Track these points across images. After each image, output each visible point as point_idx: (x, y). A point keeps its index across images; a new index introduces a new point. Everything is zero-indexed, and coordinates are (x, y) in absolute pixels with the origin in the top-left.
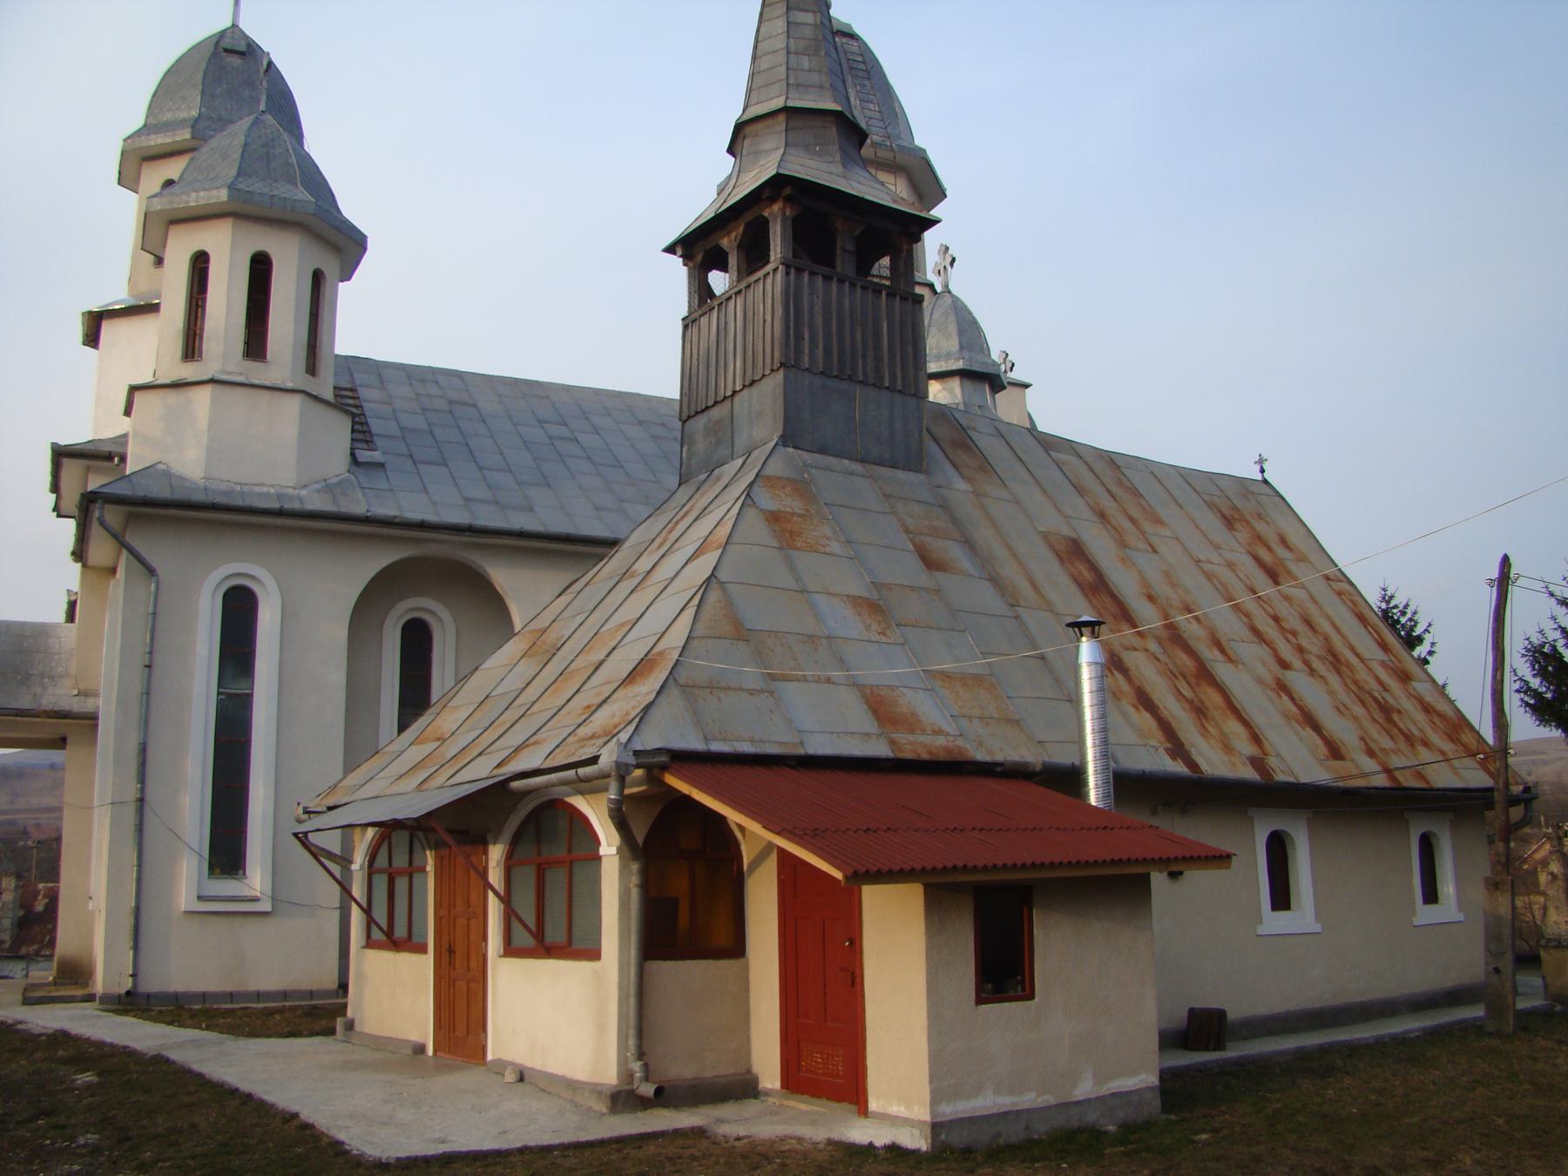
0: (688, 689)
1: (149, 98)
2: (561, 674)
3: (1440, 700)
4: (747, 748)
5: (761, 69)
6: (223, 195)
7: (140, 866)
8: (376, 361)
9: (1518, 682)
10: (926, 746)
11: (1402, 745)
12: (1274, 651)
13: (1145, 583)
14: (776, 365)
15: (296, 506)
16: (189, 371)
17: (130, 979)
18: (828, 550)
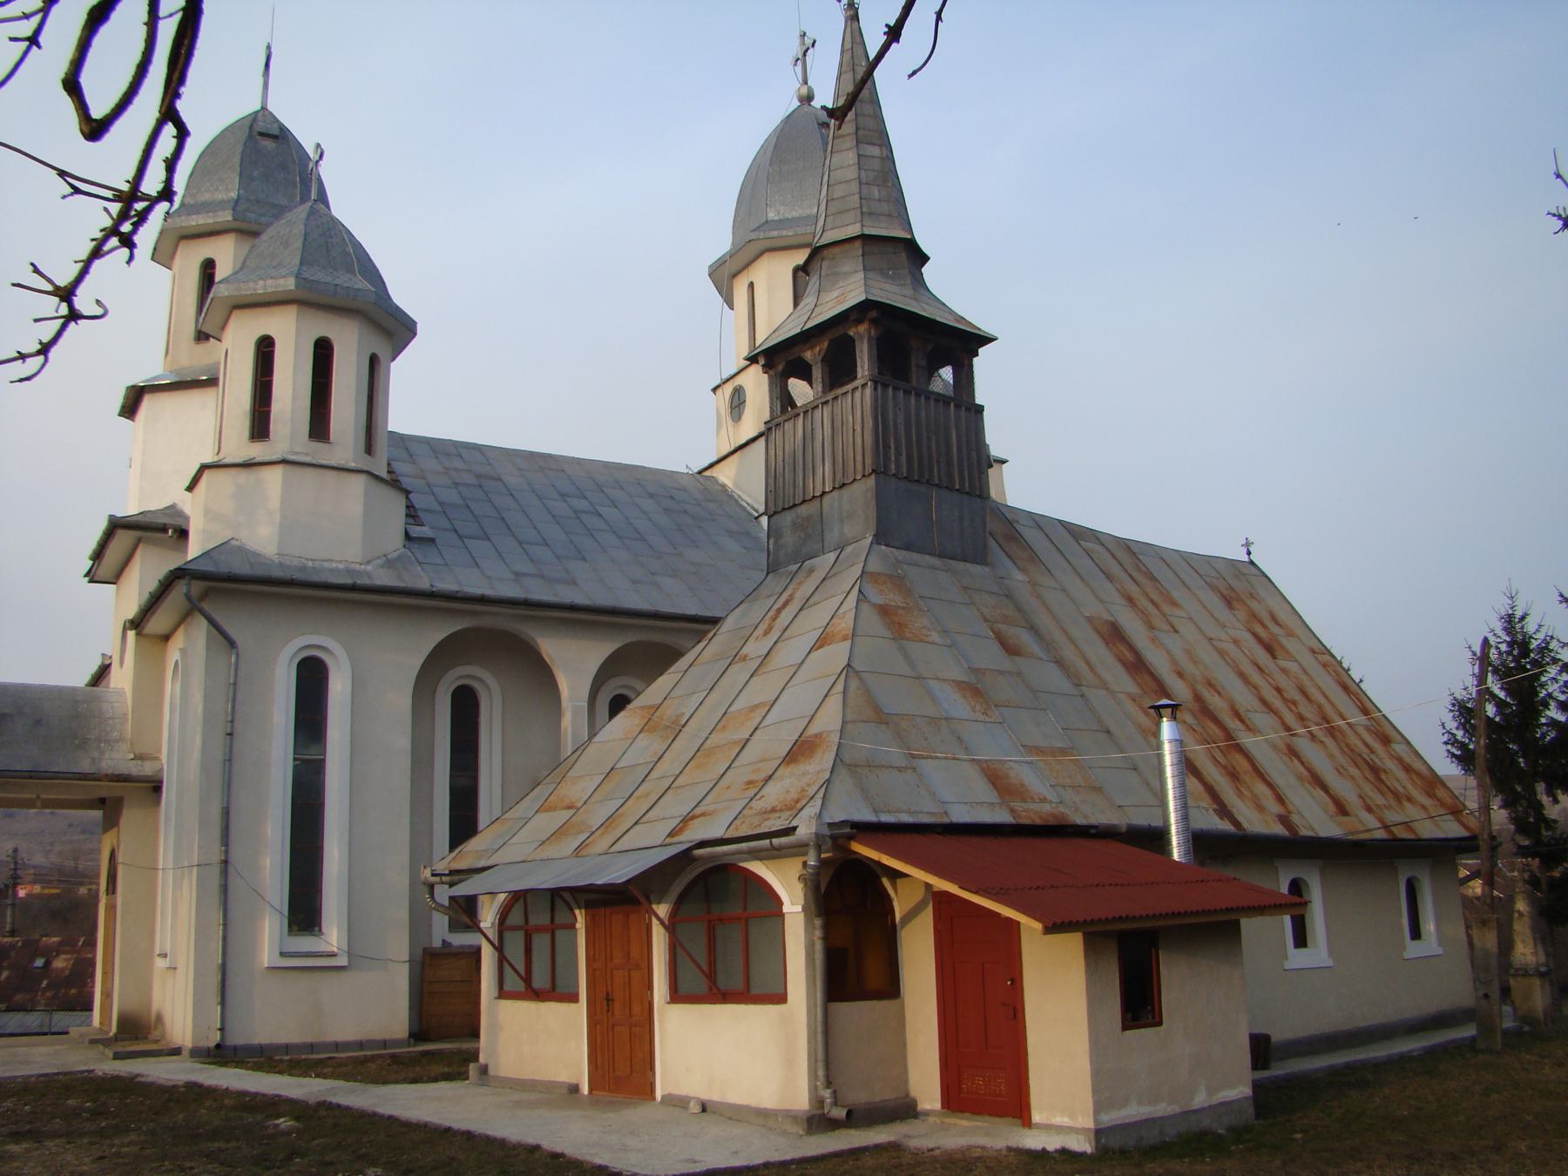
0: (852, 767)
1: (186, 178)
2: (698, 750)
3: (1416, 759)
4: (906, 818)
5: (835, 197)
6: (290, 284)
7: (225, 925)
8: (399, 434)
9: (1446, 735)
10: (1037, 812)
11: (1392, 801)
12: (1281, 718)
13: (1174, 662)
14: (868, 470)
15: (365, 581)
16: (257, 451)
17: (218, 1032)
18: (930, 639)
